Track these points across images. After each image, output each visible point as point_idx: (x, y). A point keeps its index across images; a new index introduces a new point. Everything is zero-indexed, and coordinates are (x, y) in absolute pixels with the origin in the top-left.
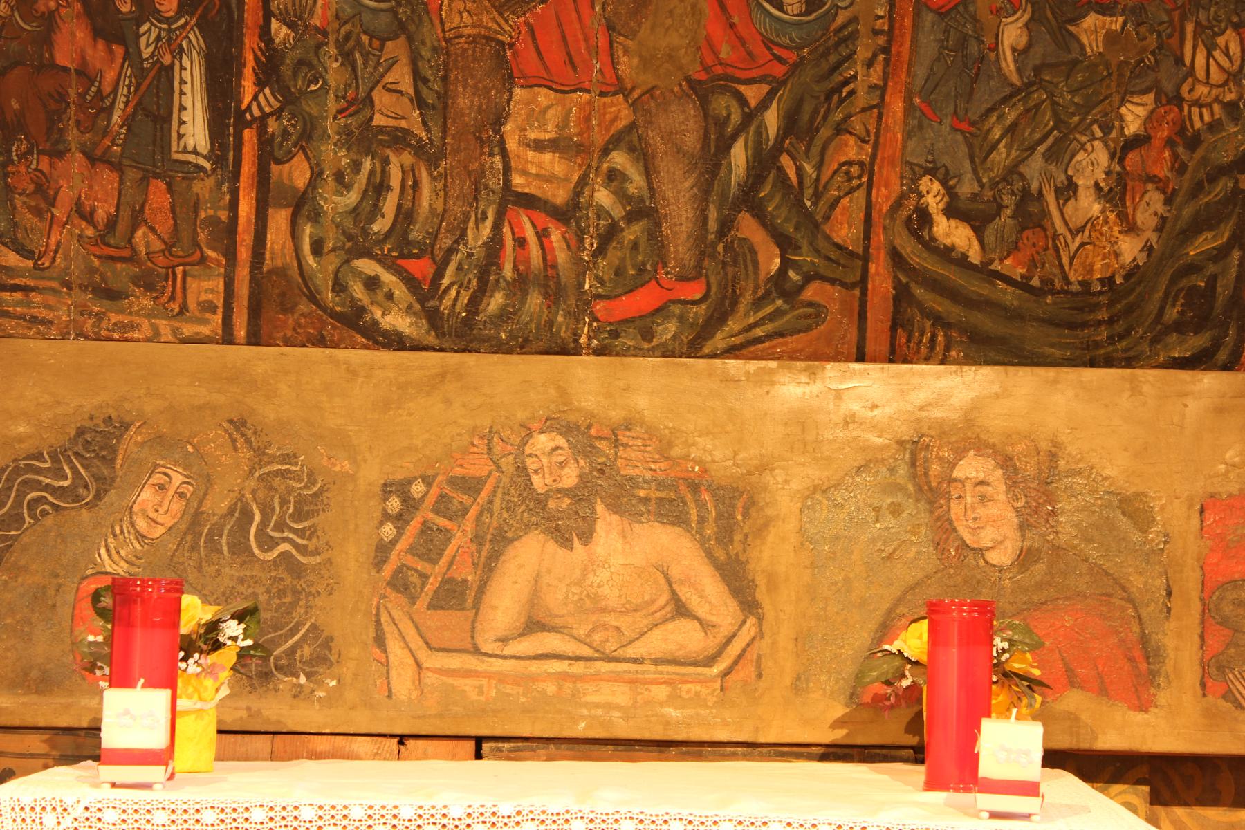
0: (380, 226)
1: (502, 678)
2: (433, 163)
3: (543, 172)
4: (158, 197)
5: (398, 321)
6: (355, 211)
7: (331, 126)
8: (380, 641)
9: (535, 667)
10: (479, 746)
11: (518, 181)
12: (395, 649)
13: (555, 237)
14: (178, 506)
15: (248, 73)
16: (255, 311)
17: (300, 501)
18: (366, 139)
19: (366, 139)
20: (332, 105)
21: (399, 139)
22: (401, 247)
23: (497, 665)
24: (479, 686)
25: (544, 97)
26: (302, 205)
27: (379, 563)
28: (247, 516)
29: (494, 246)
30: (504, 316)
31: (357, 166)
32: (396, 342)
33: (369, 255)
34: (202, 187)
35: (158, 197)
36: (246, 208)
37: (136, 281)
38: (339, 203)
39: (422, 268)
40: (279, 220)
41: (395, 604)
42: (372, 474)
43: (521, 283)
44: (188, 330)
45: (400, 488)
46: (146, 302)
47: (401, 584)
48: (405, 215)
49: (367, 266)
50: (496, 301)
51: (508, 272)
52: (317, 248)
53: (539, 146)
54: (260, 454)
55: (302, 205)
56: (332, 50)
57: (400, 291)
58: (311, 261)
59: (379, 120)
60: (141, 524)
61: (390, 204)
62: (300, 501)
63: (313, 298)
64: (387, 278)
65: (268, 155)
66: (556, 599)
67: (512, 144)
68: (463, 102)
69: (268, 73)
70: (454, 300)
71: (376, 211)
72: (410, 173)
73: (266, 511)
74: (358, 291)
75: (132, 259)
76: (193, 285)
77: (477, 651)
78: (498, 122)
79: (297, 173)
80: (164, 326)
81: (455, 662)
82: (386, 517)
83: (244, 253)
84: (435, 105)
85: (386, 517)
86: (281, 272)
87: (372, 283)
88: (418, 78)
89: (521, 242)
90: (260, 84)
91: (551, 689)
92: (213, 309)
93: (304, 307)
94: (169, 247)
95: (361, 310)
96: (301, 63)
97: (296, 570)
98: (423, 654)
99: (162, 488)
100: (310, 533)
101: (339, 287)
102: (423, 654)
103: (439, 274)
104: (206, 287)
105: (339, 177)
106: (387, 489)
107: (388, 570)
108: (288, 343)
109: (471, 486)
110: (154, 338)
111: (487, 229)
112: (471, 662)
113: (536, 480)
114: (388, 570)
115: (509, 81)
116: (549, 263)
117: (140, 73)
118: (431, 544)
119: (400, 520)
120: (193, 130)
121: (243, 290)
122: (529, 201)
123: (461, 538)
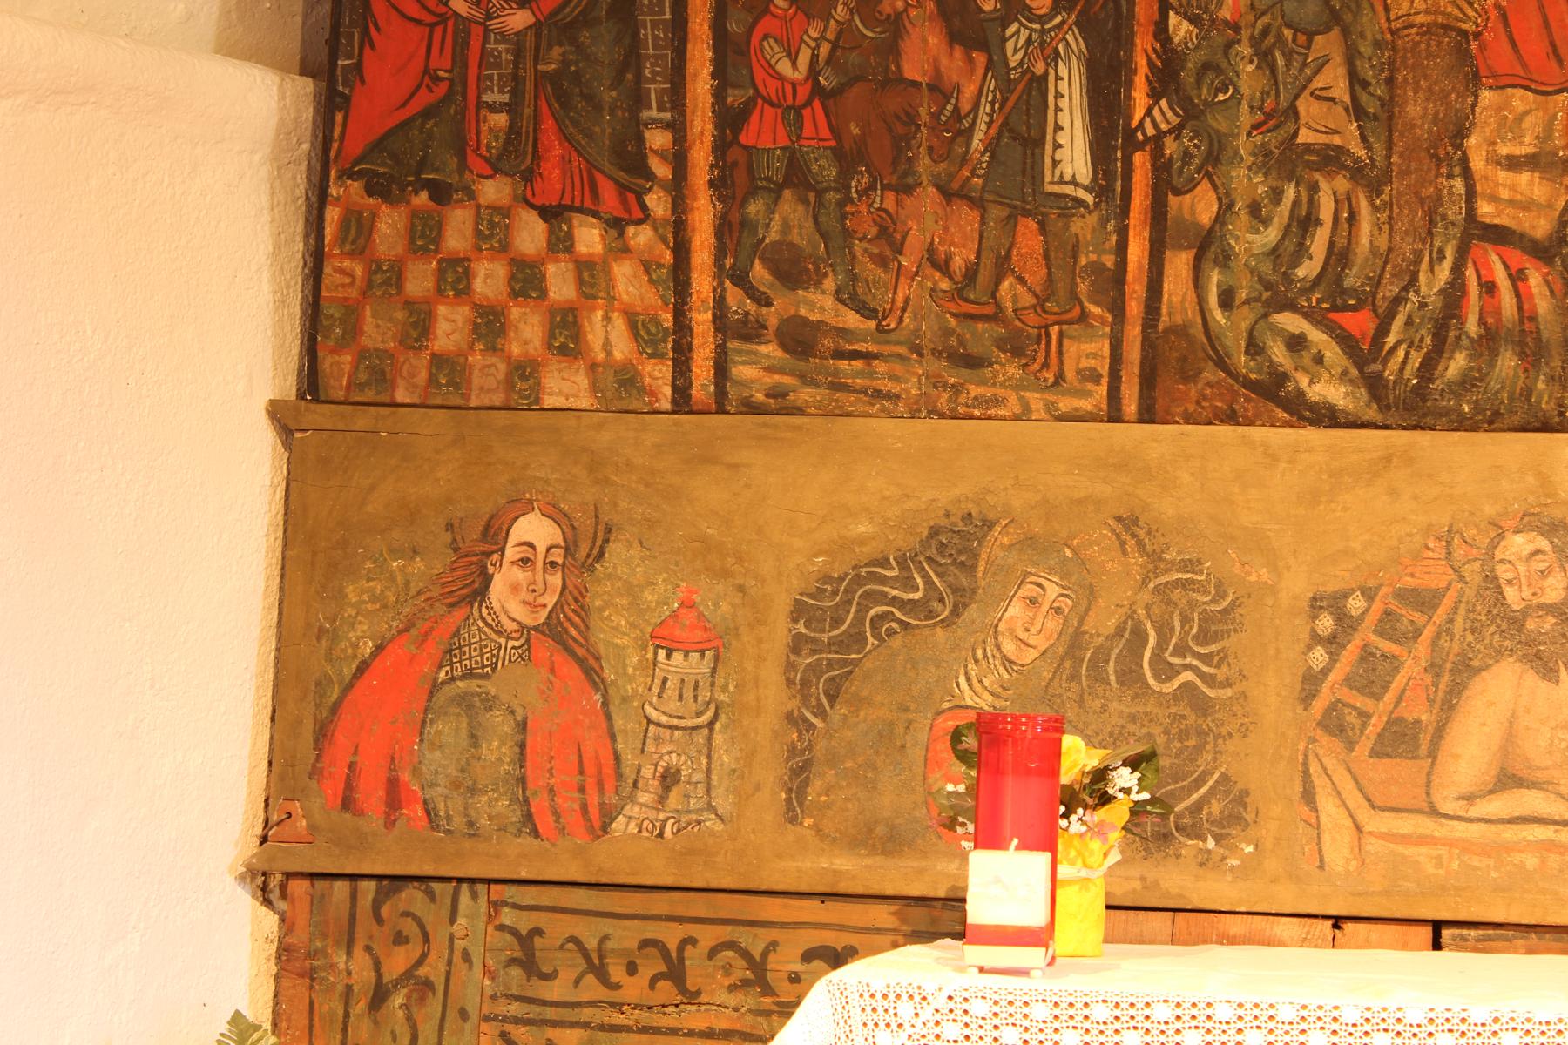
0: (1307, 270)
1: (1466, 847)
2: (1374, 189)
3: (1521, 199)
4: (1028, 238)
5: (1330, 391)
6: (1274, 252)
7: (1244, 146)
8: (1309, 796)
9: (1511, 833)
10: (1438, 933)
11: (1485, 209)
12: (1328, 806)
13: (1535, 280)
14: (1053, 624)
15: (1140, 81)
16: (1148, 380)
17: (1206, 618)
18: (1288, 161)
19: (1288, 161)
20: (1246, 119)
21: (1331, 159)
22: (1333, 297)
23: (1461, 830)
24: (1437, 868)
25: (1520, 100)
26: (1208, 246)
27: (1307, 699)
28: (1140, 637)
29: (1454, 294)
30: (1466, 383)
31: (1276, 195)
32: (1327, 417)
33: (1292, 307)
34: (1083, 226)
35: (1028, 238)
36: (1137, 251)
37: (1000, 344)
38: (1253, 241)
39: (1360, 323)
40: (1179, 264)
41: (1328, 750)
42: (1297, 585)
43: (1490, 340)
44: (1065, 404)
45: (1334, 603)
46: (1014, 370)
47: (1335, 724)
48: (1339, 256)
49: (1290, 322)
50: (1456, 365)
51: (1472, 326)
52: (1227, 300)
53: (1513, 163)
54: (1155, 559)
55: (1208, 246)
56: (1245, 49)
57: (1333, 353)
58: (1218, 316)
59: (1305, 136)
60: (1009, 647)
61: (1319, 243)
62: (1206, 618)
63: (1221, 363)
64: (1316, 336)
65: (1164, 184)
66: (1537, 748)
67: (1477, 163)
68: (1413, 110)
69: (1165, 80)
70: (1402, 363)
71: (1301, 252)
72: (1345, 202)
73: (1164, 631)
74: (1279, 353)
75: (996, 317)
76: (1071, 348)
77: (1434, 812)
78: (1460, 134)
79: (1201, 206)
80: (1036, 400)
81: (1406, 824)
82: (1316, 639)
83: (1135, 308)
84: (1374, 111)
85: (1316, 639)
86: (1181, 331)
87: (1296, 343)
88: (1356, 80)
89: (1489, 288)
90: (1155, 96)
91: (1531, 861)
92: (1096, 379)
93: (1210, 374)
94: (1041, 302)
95: (1284, 377)
96: (1206, 67)
97: (1203, 706)
98: (1364, 815)
99: (1033, 601)
100: (1221, 658)
101: (1254, 348)
102: (1364, 815)
103: (1383, 330)
104: (1087, 351)
105: (1255, 209)
106: (1317, 604)
107: (1318, 706)
108: (1189, 419)
109: (1424, 600)
110: (1023, 416)
111: (1444, 272)
112: (1426, 825)
113: (1510, 593)
114: (1318, 706)
115: (1474, 81)
116: (1526, 315)
117: (1006, 86)
118: (1373, 674)
119: (1333, 643)
120: (1072, 155)
121: (1133, 353)
122: (1499, 235)
123: (1413, 664)
